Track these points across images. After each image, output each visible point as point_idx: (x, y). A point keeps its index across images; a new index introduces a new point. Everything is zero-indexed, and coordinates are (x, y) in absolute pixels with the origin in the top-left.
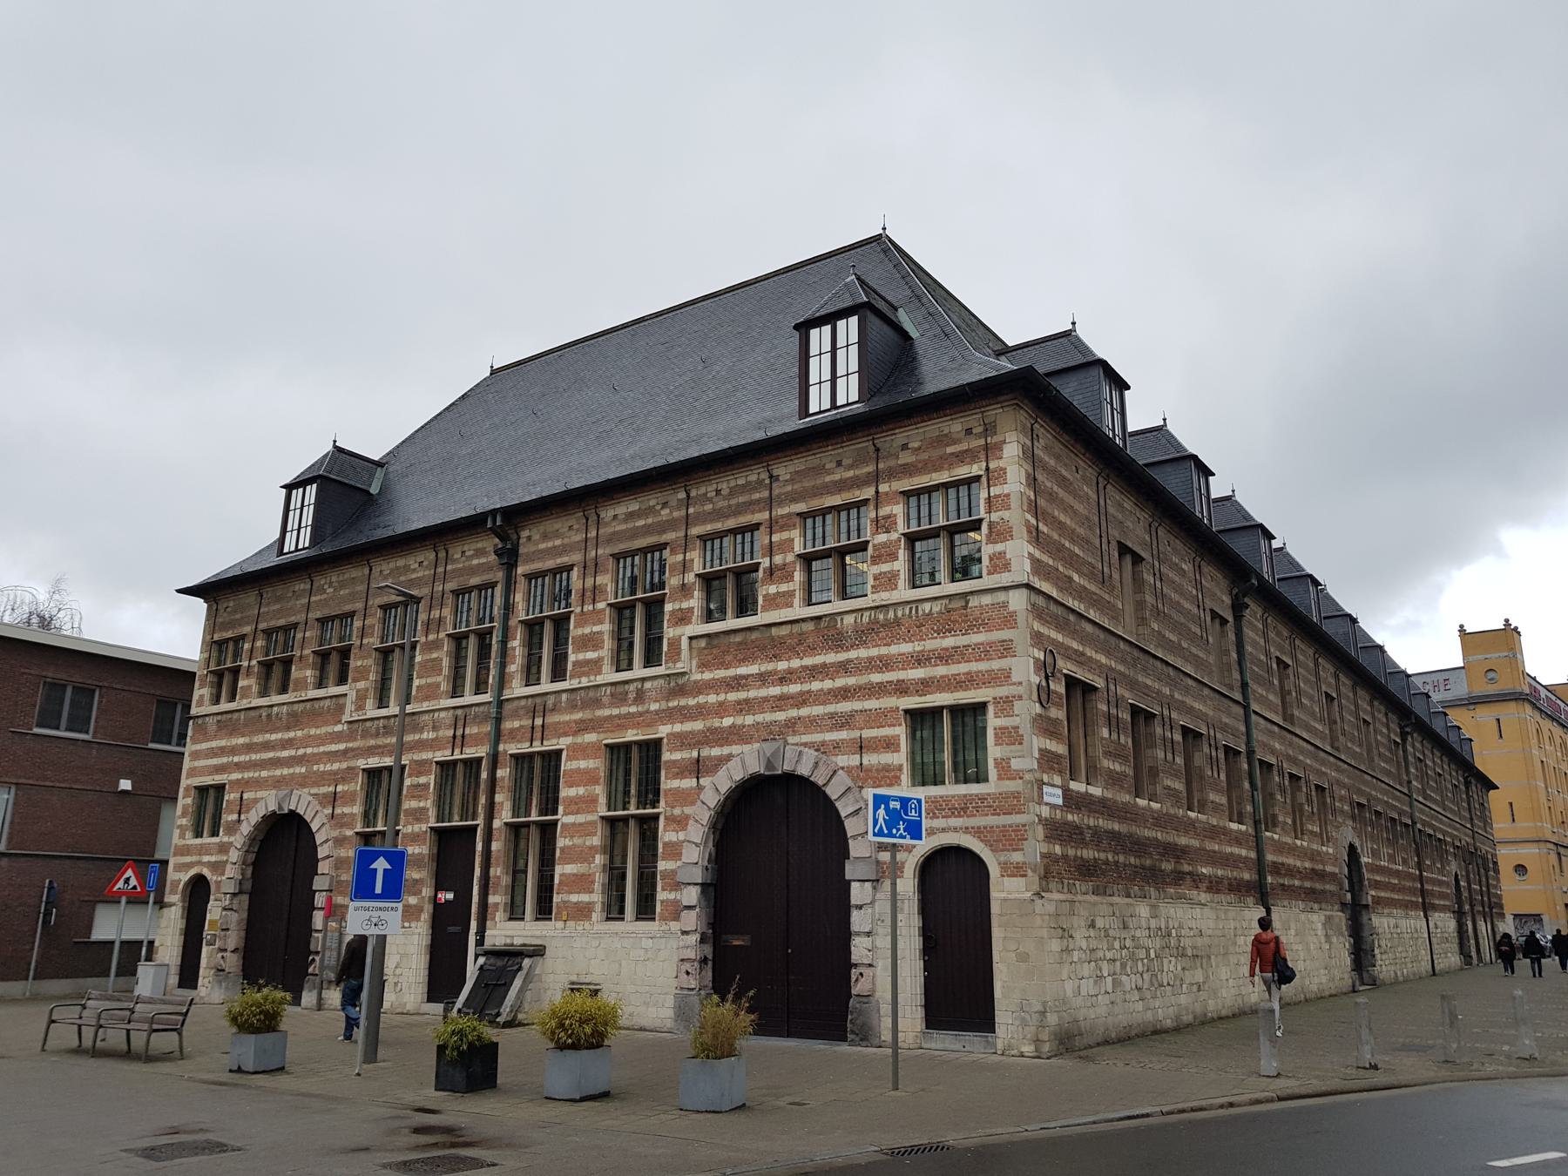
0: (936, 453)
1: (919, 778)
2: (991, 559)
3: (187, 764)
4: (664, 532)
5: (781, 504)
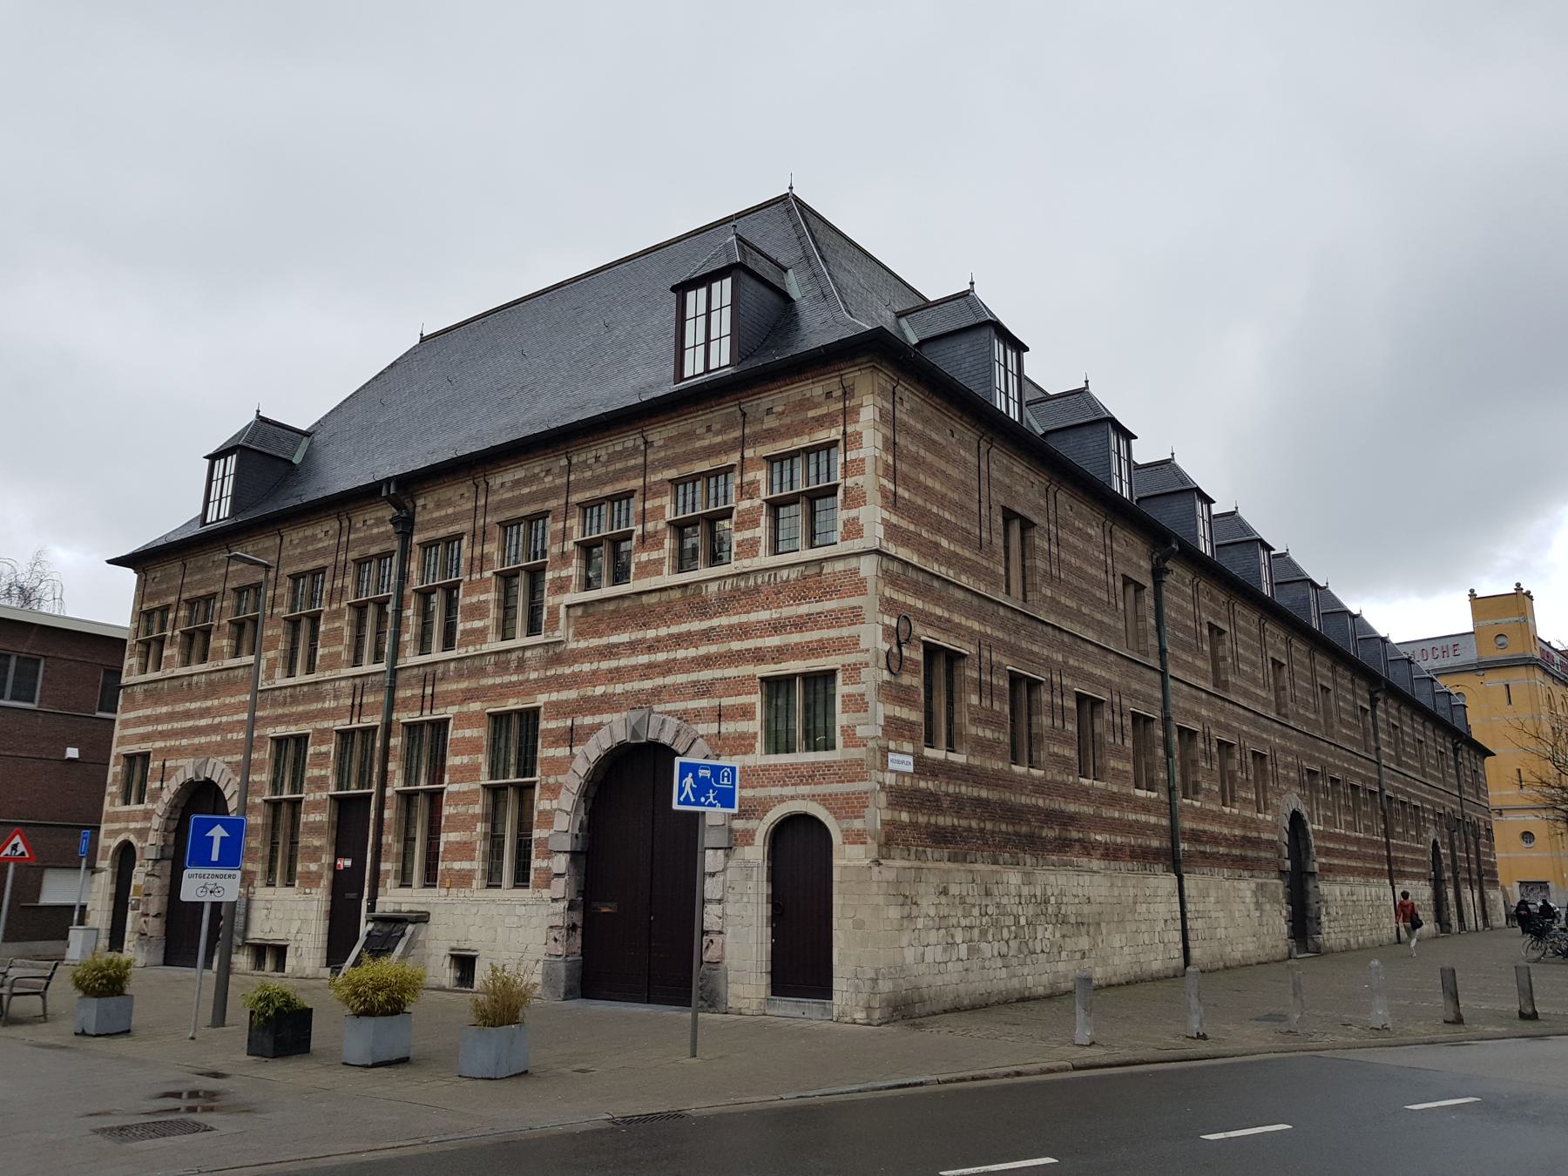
0: (797, 418)
1: (772, 745)
2: (845, 525)
3: (117, 732)
4: (546, 499)
5: (655, 470)
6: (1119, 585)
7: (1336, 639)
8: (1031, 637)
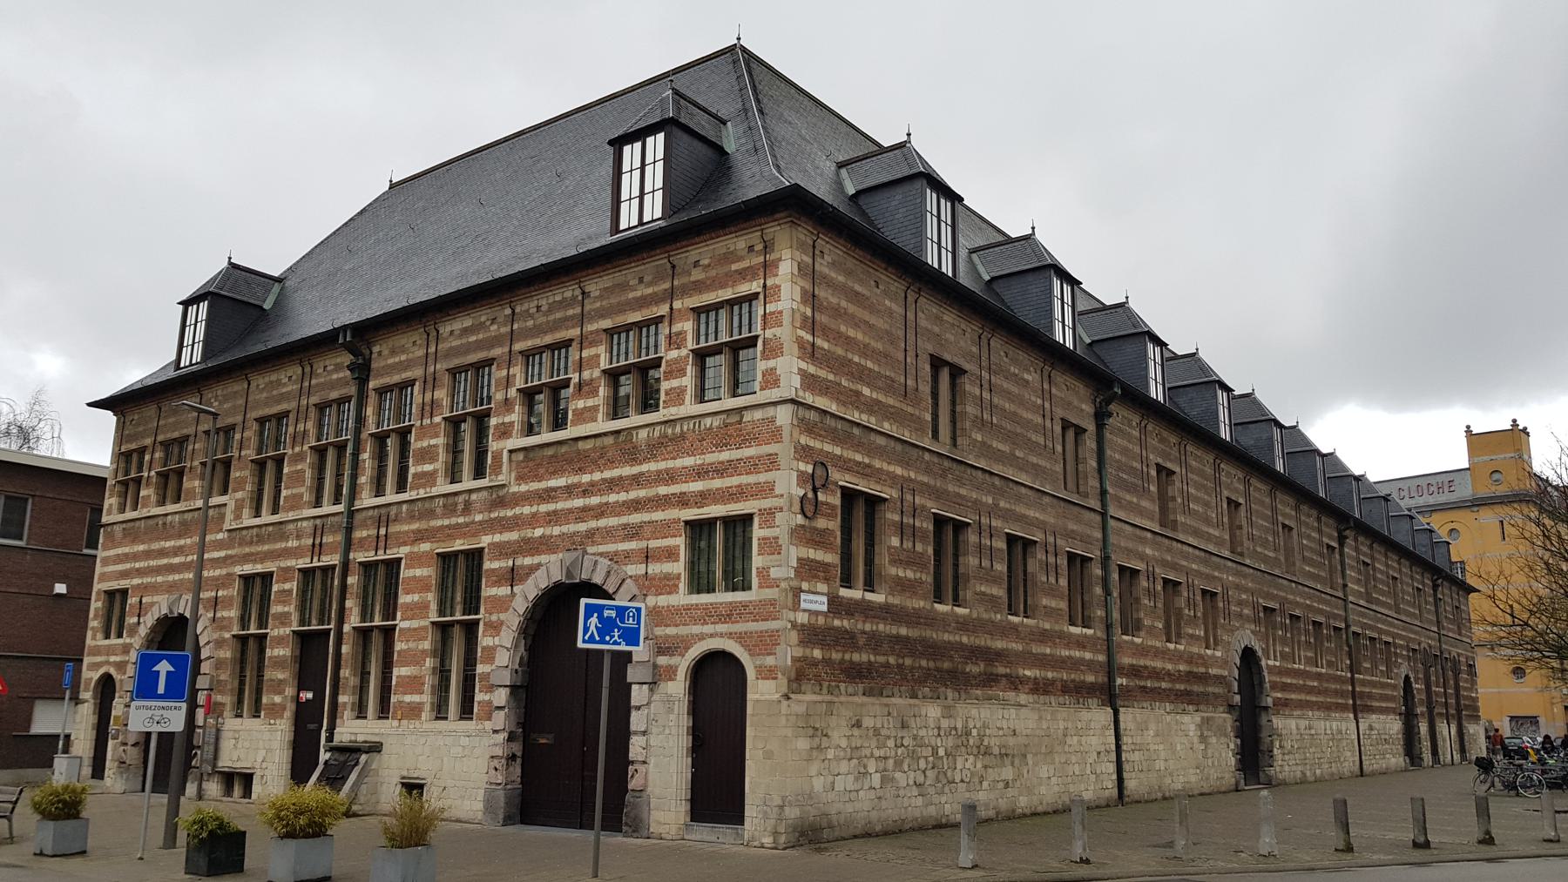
0: (722, 270)
3: (99, 569)
4: (492, 347)
5: (592, 319)
6: (1058, 429)
7: (1302, 480)
8: (959, 481)
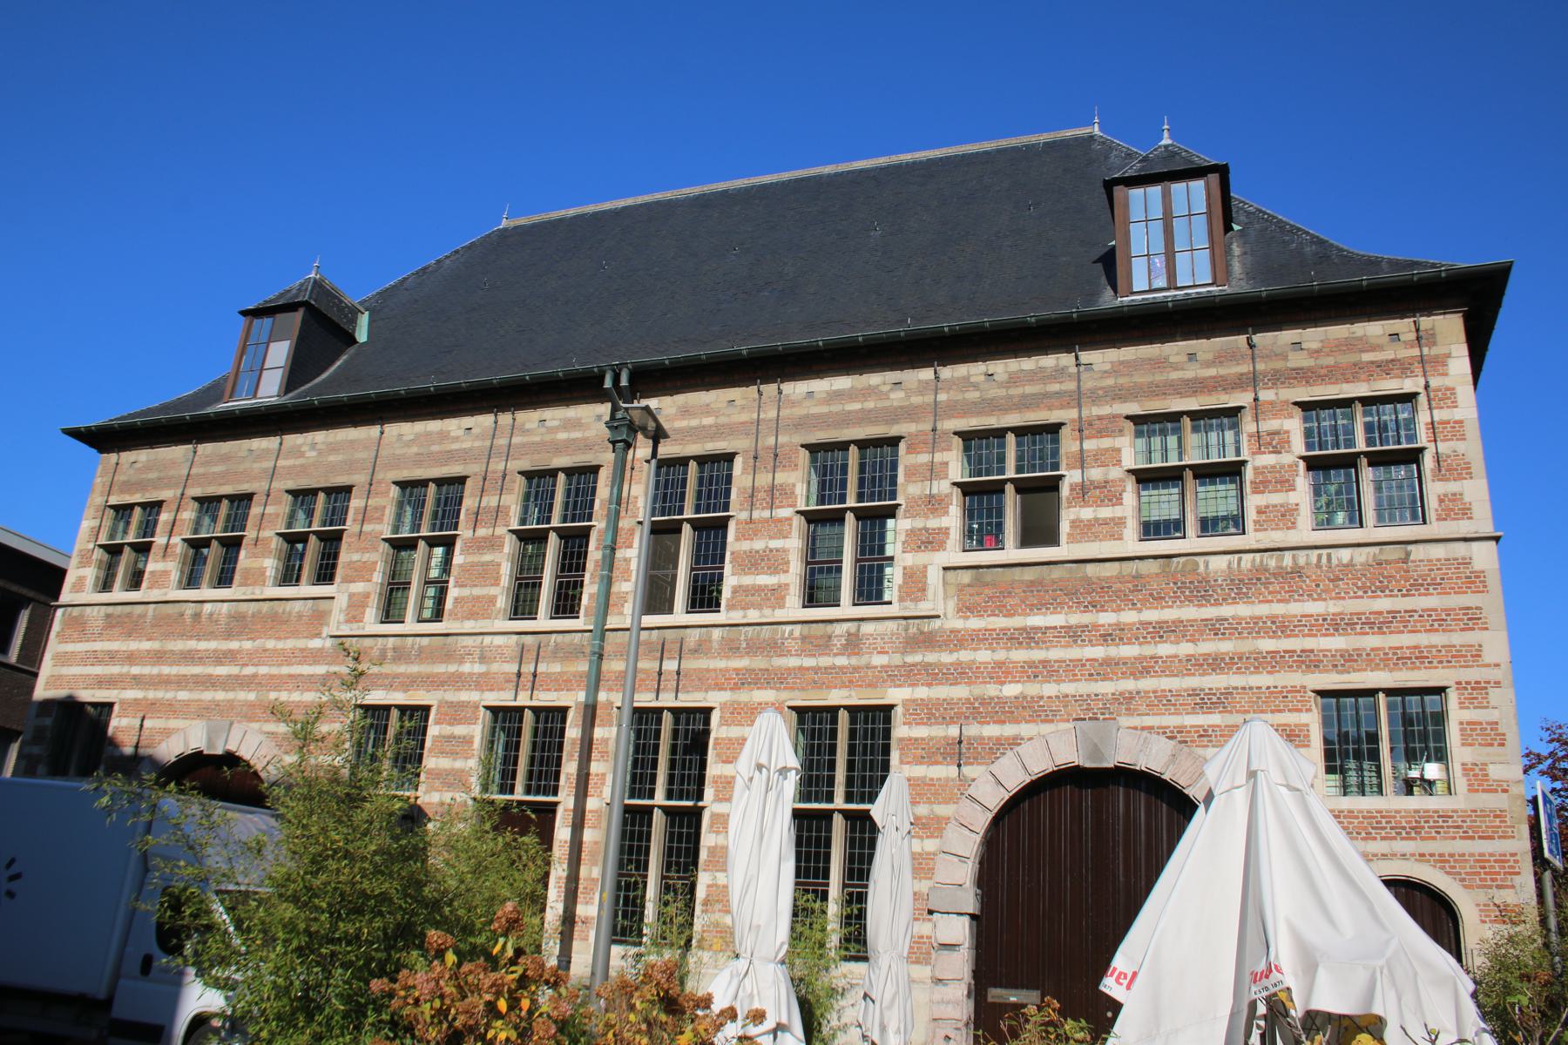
2: (1441, 501)
